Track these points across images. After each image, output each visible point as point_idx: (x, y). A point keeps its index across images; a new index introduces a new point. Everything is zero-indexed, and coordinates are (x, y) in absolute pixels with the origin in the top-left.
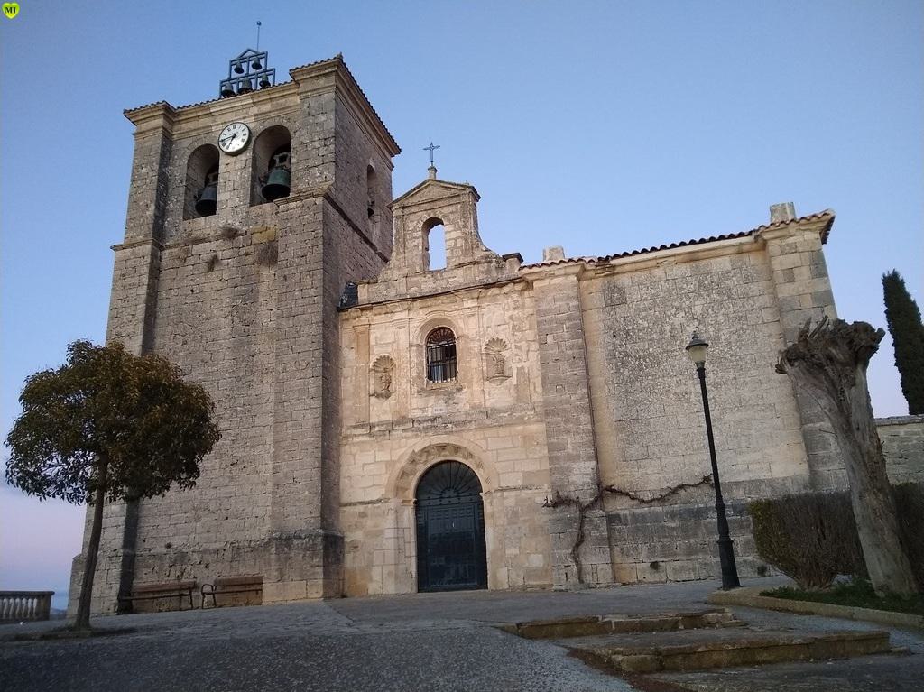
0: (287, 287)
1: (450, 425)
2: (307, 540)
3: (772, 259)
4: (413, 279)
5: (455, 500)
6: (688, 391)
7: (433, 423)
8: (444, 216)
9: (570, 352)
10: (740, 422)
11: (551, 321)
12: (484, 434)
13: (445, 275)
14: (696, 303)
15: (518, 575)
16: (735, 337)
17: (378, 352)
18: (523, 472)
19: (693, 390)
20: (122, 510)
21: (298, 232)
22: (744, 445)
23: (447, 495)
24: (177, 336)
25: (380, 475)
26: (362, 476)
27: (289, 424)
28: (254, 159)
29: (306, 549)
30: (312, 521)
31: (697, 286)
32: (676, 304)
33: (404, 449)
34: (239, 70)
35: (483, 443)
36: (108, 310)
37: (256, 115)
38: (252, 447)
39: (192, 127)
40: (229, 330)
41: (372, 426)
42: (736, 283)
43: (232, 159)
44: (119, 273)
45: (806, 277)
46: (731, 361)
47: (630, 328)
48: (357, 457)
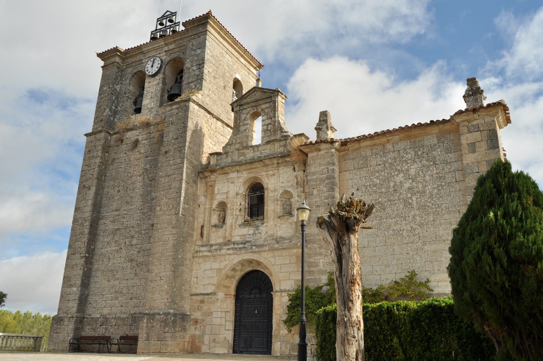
0: (167, 158)
1: (254, 247)
2: (163, 316)
3: (462, 136)
4: (241, 151)
5: (258, 296)
6: (402, 229)
7: (245, 245)
8: (263, 110)
9: (326, 201)
10: (434, 252)
11: (317, 179)
12: (274, 254)
13: (260, 148)
14: (412, 167)
15: (286, 348)
16: (436, 191)
17: (219, 198)
18: (295, 280)
19: (405, 227)
20: (77, 290)
21: (175, 124)
22: (436, 268)
23: (253, 292)
24: (115, 187)
25: (213, 277)
26: (203, 278)
27: (160, 243)
28: (164, 79)
29: (162, 322)
30: (168, 304)
31: (413, 155)
32: (399, 168)
33: (228, 262)
34: (161, 24)
35: (272, 260)
36: (80, 172)
37: (166, 51)
38: (147, 256)
39: (133, 61)
40: (141, 184)
41: (212, 246)
42: (439, 153)
43: (152, 79)
44: (88, 150)
45: (484, 149)
46: (432, 208)
47: (368, 184)
48: (202, 265)
